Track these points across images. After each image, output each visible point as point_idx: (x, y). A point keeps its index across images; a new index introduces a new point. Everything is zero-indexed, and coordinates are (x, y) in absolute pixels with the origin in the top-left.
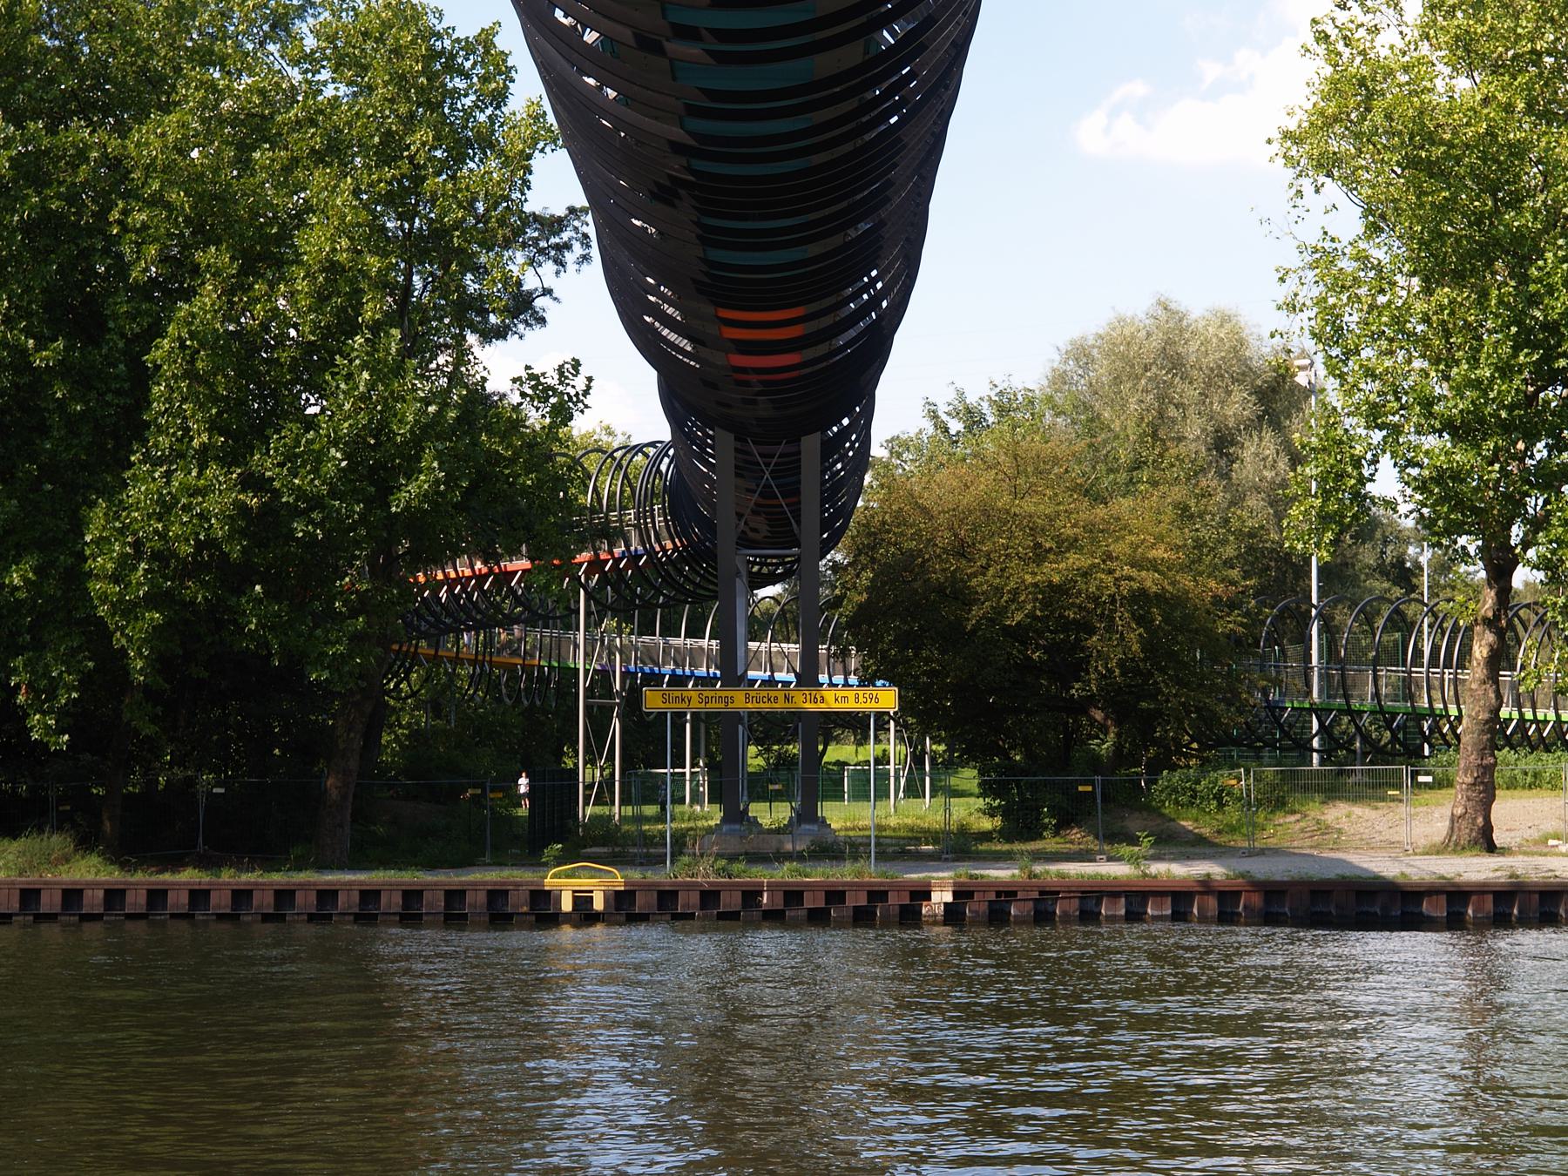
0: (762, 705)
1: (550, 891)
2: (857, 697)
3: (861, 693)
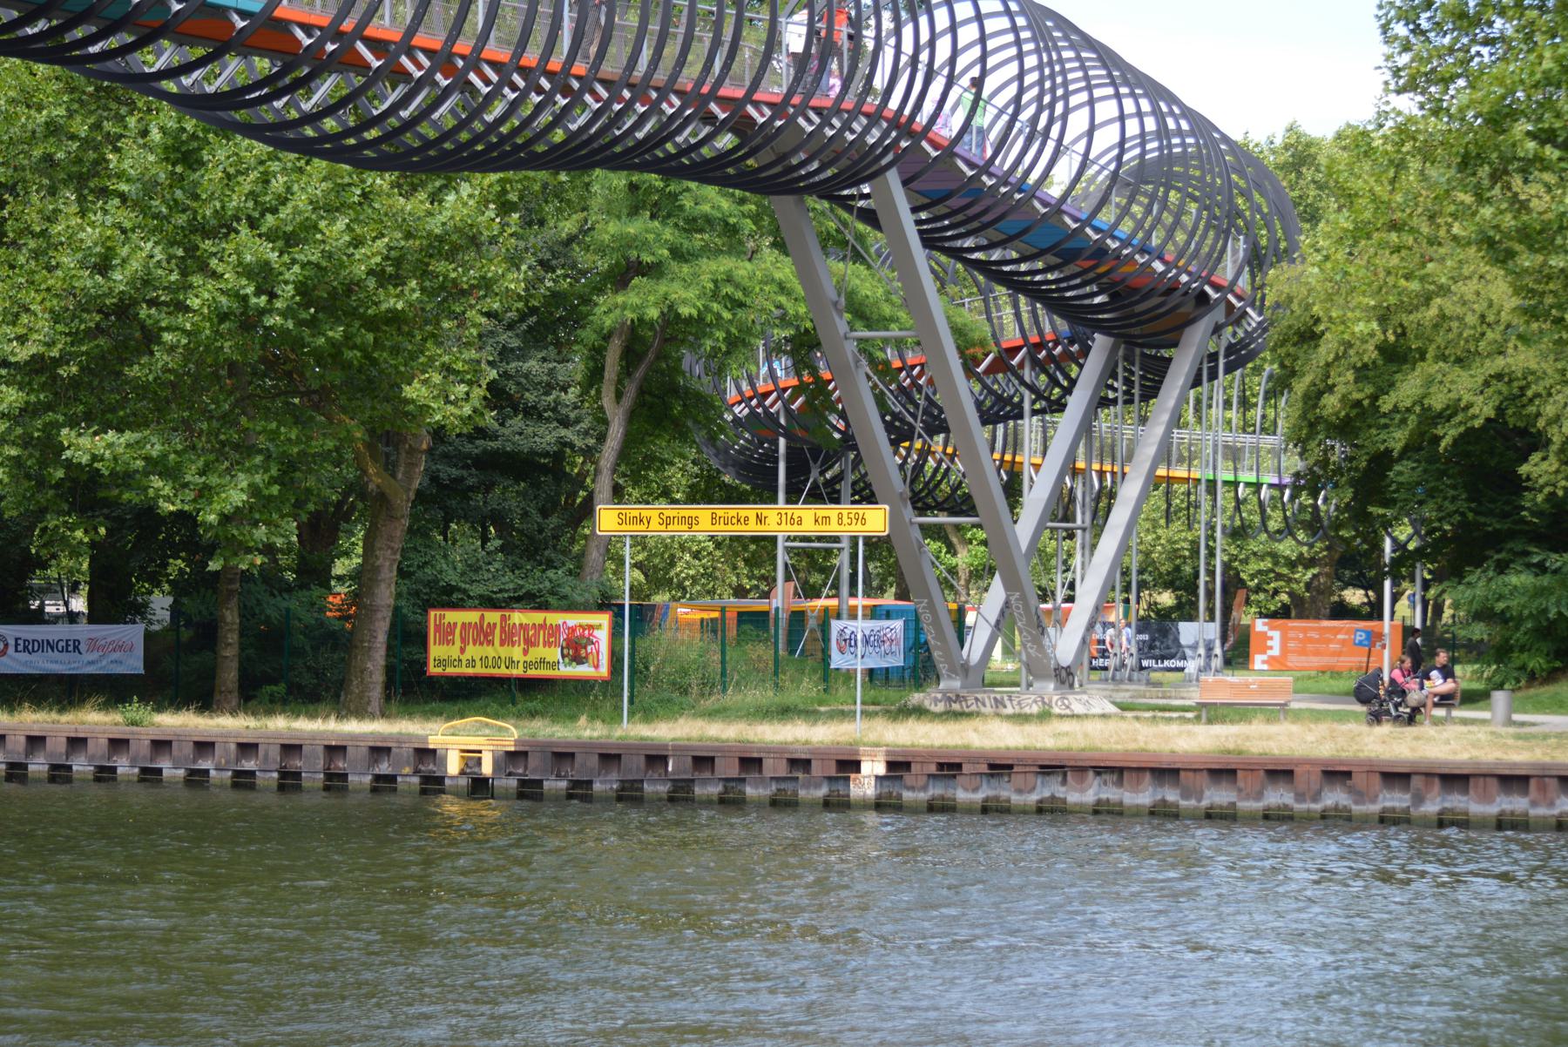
0: (730, 527)
1: (434, 751)
2: (840, 518)
3: (845, 512)
